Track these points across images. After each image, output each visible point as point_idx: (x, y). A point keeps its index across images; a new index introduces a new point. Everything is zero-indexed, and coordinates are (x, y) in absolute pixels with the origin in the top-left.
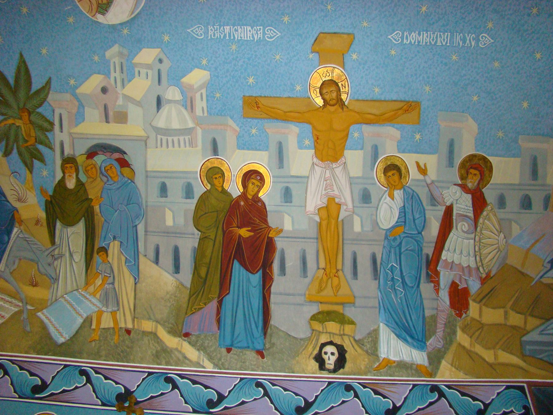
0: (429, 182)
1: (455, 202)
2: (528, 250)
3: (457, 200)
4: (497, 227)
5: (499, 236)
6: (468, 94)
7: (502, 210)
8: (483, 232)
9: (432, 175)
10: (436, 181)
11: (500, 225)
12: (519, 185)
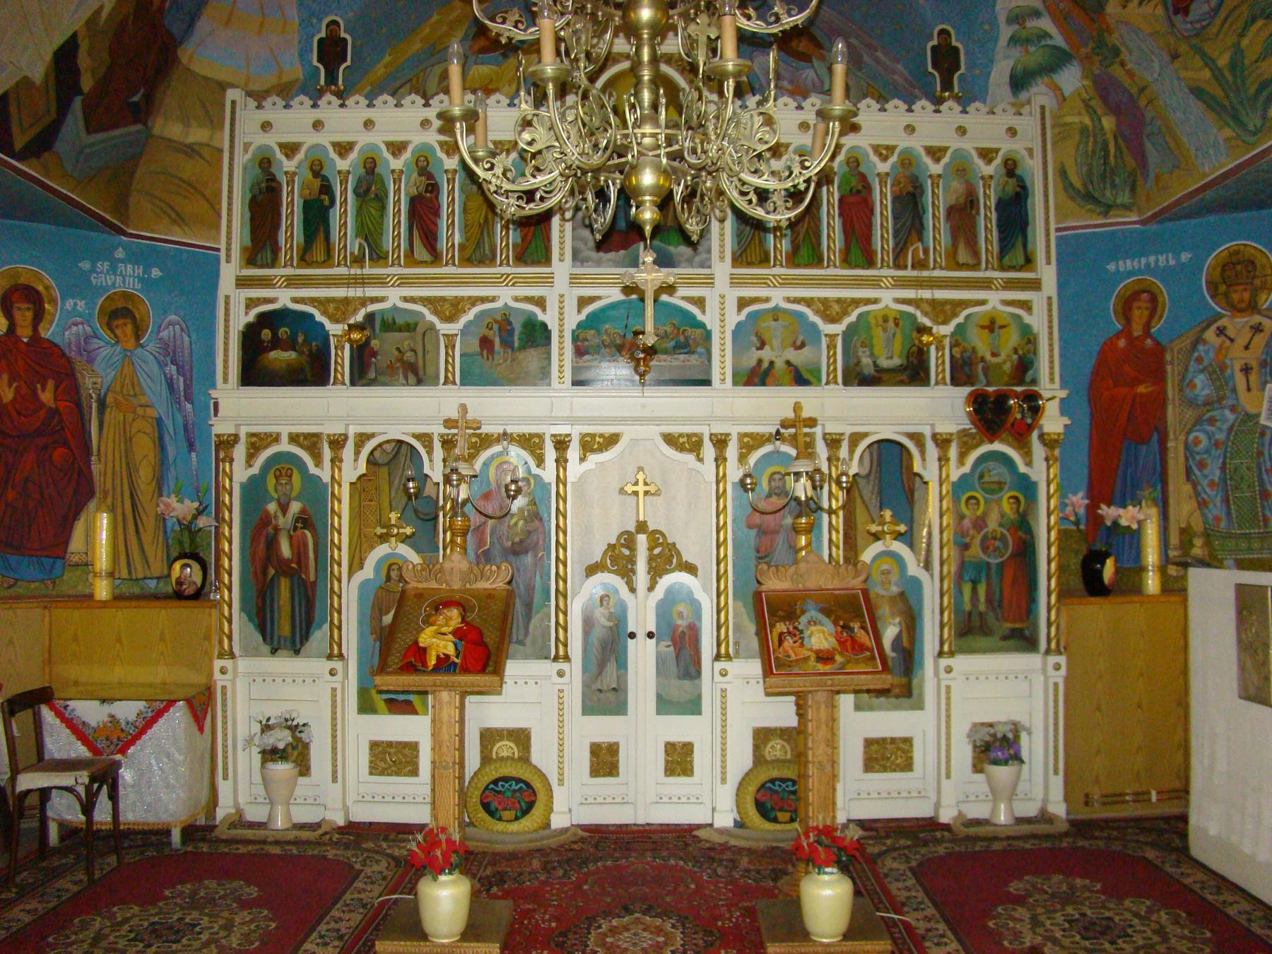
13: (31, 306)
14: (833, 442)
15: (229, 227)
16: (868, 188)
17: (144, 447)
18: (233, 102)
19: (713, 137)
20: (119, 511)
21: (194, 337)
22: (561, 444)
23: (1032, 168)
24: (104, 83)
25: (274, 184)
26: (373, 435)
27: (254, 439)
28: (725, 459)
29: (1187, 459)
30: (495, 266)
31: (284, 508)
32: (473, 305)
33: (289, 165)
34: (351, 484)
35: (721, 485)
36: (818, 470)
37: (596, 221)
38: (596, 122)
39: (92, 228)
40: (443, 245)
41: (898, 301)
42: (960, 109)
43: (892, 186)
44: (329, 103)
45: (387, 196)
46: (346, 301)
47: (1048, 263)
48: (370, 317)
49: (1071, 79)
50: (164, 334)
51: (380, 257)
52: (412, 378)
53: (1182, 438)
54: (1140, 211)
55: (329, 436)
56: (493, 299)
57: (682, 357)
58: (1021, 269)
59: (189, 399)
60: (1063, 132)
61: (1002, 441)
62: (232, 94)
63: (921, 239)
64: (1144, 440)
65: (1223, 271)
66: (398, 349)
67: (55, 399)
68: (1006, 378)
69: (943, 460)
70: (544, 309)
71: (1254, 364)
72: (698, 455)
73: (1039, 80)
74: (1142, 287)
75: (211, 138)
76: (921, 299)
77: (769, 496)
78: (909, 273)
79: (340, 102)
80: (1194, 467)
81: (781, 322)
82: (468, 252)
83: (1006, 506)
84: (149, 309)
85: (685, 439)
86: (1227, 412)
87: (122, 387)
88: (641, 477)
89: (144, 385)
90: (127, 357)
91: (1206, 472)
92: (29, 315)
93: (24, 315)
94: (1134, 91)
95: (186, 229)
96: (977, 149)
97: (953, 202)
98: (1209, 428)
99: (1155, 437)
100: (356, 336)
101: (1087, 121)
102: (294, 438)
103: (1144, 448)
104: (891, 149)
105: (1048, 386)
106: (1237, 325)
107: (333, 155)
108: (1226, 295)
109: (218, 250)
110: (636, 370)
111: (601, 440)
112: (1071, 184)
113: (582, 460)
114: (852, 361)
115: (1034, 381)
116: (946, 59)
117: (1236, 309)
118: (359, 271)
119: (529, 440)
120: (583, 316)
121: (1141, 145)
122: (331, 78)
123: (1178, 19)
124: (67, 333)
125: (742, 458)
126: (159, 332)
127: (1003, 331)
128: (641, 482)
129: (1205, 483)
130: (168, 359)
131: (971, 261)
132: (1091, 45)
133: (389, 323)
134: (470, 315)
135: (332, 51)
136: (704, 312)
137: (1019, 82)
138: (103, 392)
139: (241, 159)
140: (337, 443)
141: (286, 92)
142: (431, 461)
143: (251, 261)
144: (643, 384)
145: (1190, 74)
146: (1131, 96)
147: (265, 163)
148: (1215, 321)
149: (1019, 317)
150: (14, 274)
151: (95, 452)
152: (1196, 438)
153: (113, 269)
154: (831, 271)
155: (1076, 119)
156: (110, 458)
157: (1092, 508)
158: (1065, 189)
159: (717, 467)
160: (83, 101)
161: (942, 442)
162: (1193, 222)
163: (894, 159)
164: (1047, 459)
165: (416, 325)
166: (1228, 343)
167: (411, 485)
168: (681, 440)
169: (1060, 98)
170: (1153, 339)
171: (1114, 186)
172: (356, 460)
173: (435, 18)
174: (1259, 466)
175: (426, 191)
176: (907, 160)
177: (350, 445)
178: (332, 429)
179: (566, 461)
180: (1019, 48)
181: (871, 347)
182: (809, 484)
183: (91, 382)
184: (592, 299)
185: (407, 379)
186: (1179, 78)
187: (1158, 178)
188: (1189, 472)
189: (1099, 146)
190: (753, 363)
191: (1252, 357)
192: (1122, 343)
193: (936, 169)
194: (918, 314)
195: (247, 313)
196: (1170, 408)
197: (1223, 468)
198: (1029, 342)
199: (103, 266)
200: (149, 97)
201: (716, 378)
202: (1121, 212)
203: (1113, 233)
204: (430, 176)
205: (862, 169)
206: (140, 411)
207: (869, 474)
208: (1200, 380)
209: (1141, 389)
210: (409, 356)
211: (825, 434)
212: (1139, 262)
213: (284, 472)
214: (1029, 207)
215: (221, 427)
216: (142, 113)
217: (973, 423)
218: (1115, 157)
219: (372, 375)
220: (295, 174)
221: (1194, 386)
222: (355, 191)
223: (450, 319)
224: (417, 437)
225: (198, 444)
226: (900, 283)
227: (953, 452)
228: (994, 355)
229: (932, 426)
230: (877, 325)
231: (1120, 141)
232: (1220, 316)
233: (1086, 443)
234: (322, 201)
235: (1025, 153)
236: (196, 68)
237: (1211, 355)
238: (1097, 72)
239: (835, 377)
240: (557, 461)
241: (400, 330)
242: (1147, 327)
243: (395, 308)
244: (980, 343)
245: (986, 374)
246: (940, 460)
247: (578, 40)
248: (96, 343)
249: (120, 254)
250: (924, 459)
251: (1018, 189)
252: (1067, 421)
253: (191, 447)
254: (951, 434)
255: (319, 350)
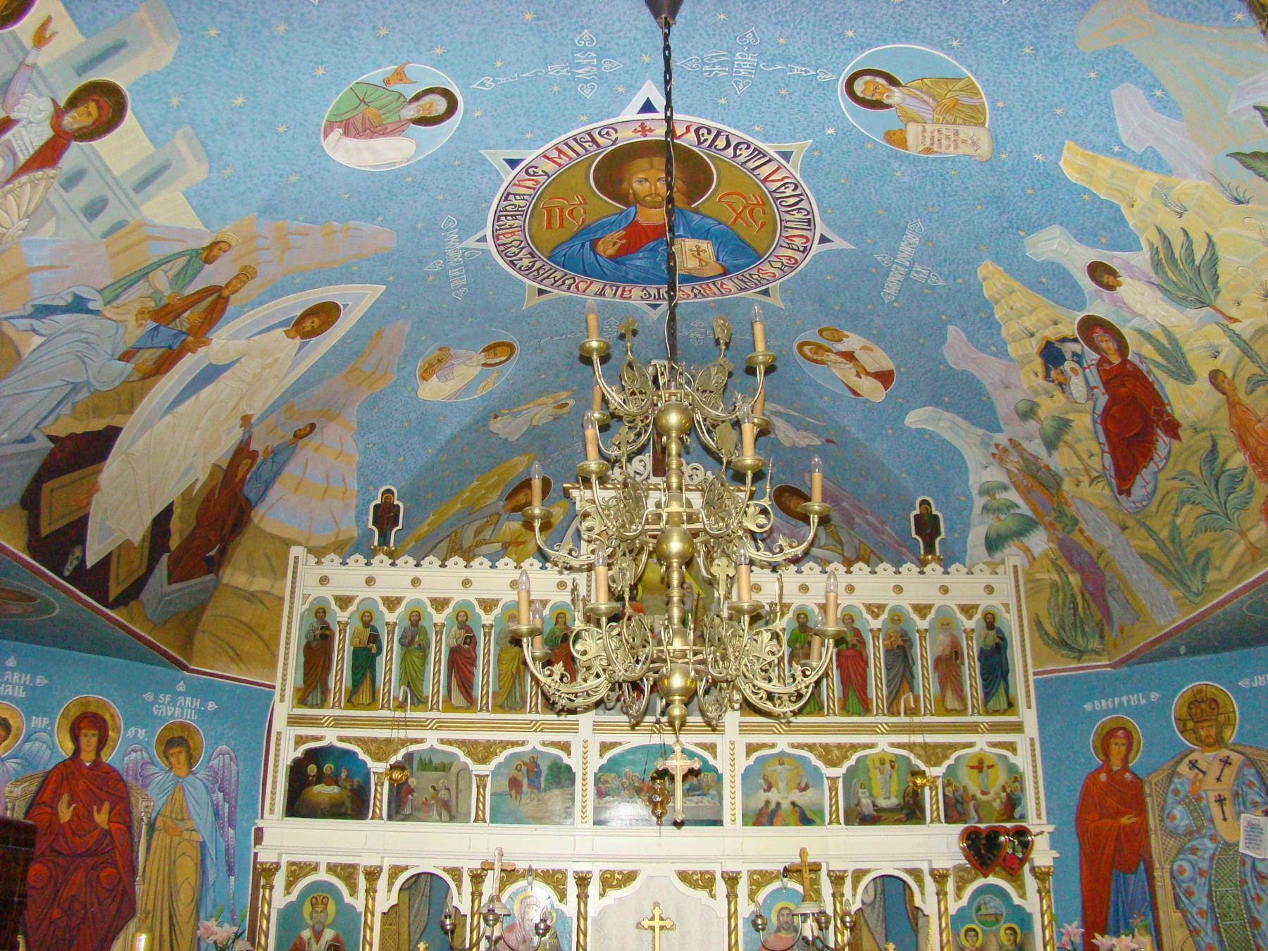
0: (30, 61)
1: (24, 122)
2: (32, 270)
3: (31, 122)
4: (32, 206)
5: (20, 220)
6: (213, 19)
7: (62, 191)
8: (10, 197)
9: (43, 58)
10: (40, 73)
11: (37, 208)
12: (114, 178)
13: (96, 732)
14: (837, 879)
15: (285, 669)
16: (863, 642)
17: (187, 869)
18: (296, 558)
19: (732, 658)
20: (157, 933)
21: (242, 766)
22: (583, 881)
23: (1010, 622)
24: (187, 543)
25: (327, 632)
26: (406, 868)
27: (294, 868)
28: (736, 896)
29: (1174, 888)
30: (524, 712)
31: (318, 935)
32: (505, 748)
33: (342, 616)
34: (384, 913)
35: (733, 920)
36: (823, 913)
37: (631, 709)
38: (638, 642)
39: (159, 664)
40: (478, 692)
41: (892, 745)
42: (942, 570)
43: (884, 640)
44: (382, 562)
45: (429, 646)
46: (388, 741)
47: (1029, 707)
48: (409, 757)
49: (1039, 541)
50: (215, 763)
51: (420, 702)
52: (445, 815)
53: (1167, 866)
54: (1110, 656)
55: (365, 867)
56: (523, 743)
57: (695, 799)
58: (1004, 713)
59: (231, 825)
60: (1034, 587)
61: (996, 874)
62: (296, 551)
63: (912, 690)
64: (1132, 869)
65: (1189, 708)
66: (433, 787)
67: (110, 821)
68: (996, 815)
69: (941, 894)
70: (569, 754)
71: (1227, 795)
72: (711, 892)
73: (1011, 543)
74: (1119, 725)
75: (273, 586)
76: (914, 744)
77: (778, 930)
78: (903, 719)
79: (391, 561)
80: (1181, 895)
81: (786, 766)
82: (500, 700)
83: (1004, 937)
84: (203, 738)
85: (699, 877)
86: (1207, 841)
87: (171, 811)
88: (657, 912)
89: (190, 806)
90: (178, 784)
91: (1193, 899)
92: (94, 740)
93: (89, 740)
94: (1094, 554)
95: (242, 665)
96: (959, 606)
97: (939, 653)
98: (1191, 857)
99: (1142, 866)
100: (396, 775)
101: (1056, 577)
102: (332, 868)
103: (1132, 877)
104: (881, 607)
105: (1036, 821)
106: (1207, 758)
107: (382, 608)
108: (1195, 731)
109: (274, 687)
110: (654, 813)
111: (620, 877)
112: (1046, 633)
113: (602, 895)
114: (853, 802)
115: (1022, 817)
116: (928, 526)
117: (1205, 744)
118: (403, 715)
119: (552, 876)
120: (604, 760)
121: (1105, 600)
122: (384, 539)
123: (1123, 498)
124: (126, 758)
125: (752, 896)
126: (210, 760)
127: (990, 770)
128: (657, 918)
129: (1194, 910)
130: (216, 787)
131: (957, 706)
132: (1054, 514)
133: (430, 763)
134: (501, 758)
135: (386, 516)
136: (715, 757)
137: (993, 544)
138: (153, 815)
139: (300, 608)
140: (372, 875)
141: (344, 549)
142: (459, 894)
143: (302, 701)
144: (659, 824)
145: (1137, 542)
146: (1091, 558)
147: (321, 613)
148: (1187, 755)
149: (1005, 757)
150: (86, 702)
151: (140, 873)
152: (1180, 866)
153: (173, 702)
154: (831, 719)
155: (1046, 576)
156: (153, 882)
157: (1087, 937)
158: (1041, 637)
159: (729, 903)
160: (169, 557)
161: (940, 877)
162: (1158, 665)
163: (884, 616)
164: (1039, 891)
165: (451, 765)
166: (1201, 775)
167: (448, 921)
168: (695, 877)
169: (1031, 559)
170: (1131, 772)
171: (1084, 633)
172: (389, 891)
173: (476, 483)
174: (1244, 894)
175: (465, 643)
176: (897, 617)
177: (384, 877)
178: (367, 861)
179: (587, 896)
180: (991, 516)
181: (870, 789)
182: (815, 925)
183: (142, 807)
184: (613, 745)
185: (440, 815)
186: (1130, 546)
187: (1122, 629)
188: (1176, 898)
189: (1068, 601)
190: (761, 804)
191: (1225, 788)
192: (1103, 777)
193: (923, 624)
194: (912, 757)
195: (295, 749)
196: (1153, 837)
197: (1210, 896)
198: (1016, 779)
199: (165, 698)
200: (223, 553)
201: (727, 818)
202: (1092, 657)
203: (1086, 676)
204: (469, 630)
205: (856, 625)
206: (186, 834)
207: (874, 902)
208: (1178, 811)
209: (1125, 820)
210: (443, 794)
211: (829, 872)
212: (1113, 702)
213: (320, 901)
214: (1008, 657)
215: (266, 856)
216: (214, 565)
217: (967, 858)
218: (1083, 608)
219: (408, 811)
220: (347, 624)
221: (1174, 817)
222: (401, 643)
223: (483, 760)
224: (448, 870)
225: (236, 870)
226: (895, 729)
227: (950, 886)
228: (984, 793)
229: (930, 861)
230: (875, 768)
231: (1088, 596)
232: (1193, 751)
233: (1077, 873)
234: (370, 649)
235: (1002, 608)
236: (263, 526)
237: (1187, 787)
238: (1060, 536)
239: (838, 816)
240: (578, 896)
241: (436, 769)
242: (1125, 761)
243: (432, 749)
244: (970, 782)
245: (976, 810)
246: (938, 894)
247: (624, 575)
248: (153, 769)
249: (181, 687)
250: (923, 894)
251: (998, 640)
252: (1055, 854)
253: (230, 870)
254: (947, 870)
255: (360, 787)
